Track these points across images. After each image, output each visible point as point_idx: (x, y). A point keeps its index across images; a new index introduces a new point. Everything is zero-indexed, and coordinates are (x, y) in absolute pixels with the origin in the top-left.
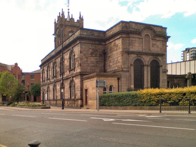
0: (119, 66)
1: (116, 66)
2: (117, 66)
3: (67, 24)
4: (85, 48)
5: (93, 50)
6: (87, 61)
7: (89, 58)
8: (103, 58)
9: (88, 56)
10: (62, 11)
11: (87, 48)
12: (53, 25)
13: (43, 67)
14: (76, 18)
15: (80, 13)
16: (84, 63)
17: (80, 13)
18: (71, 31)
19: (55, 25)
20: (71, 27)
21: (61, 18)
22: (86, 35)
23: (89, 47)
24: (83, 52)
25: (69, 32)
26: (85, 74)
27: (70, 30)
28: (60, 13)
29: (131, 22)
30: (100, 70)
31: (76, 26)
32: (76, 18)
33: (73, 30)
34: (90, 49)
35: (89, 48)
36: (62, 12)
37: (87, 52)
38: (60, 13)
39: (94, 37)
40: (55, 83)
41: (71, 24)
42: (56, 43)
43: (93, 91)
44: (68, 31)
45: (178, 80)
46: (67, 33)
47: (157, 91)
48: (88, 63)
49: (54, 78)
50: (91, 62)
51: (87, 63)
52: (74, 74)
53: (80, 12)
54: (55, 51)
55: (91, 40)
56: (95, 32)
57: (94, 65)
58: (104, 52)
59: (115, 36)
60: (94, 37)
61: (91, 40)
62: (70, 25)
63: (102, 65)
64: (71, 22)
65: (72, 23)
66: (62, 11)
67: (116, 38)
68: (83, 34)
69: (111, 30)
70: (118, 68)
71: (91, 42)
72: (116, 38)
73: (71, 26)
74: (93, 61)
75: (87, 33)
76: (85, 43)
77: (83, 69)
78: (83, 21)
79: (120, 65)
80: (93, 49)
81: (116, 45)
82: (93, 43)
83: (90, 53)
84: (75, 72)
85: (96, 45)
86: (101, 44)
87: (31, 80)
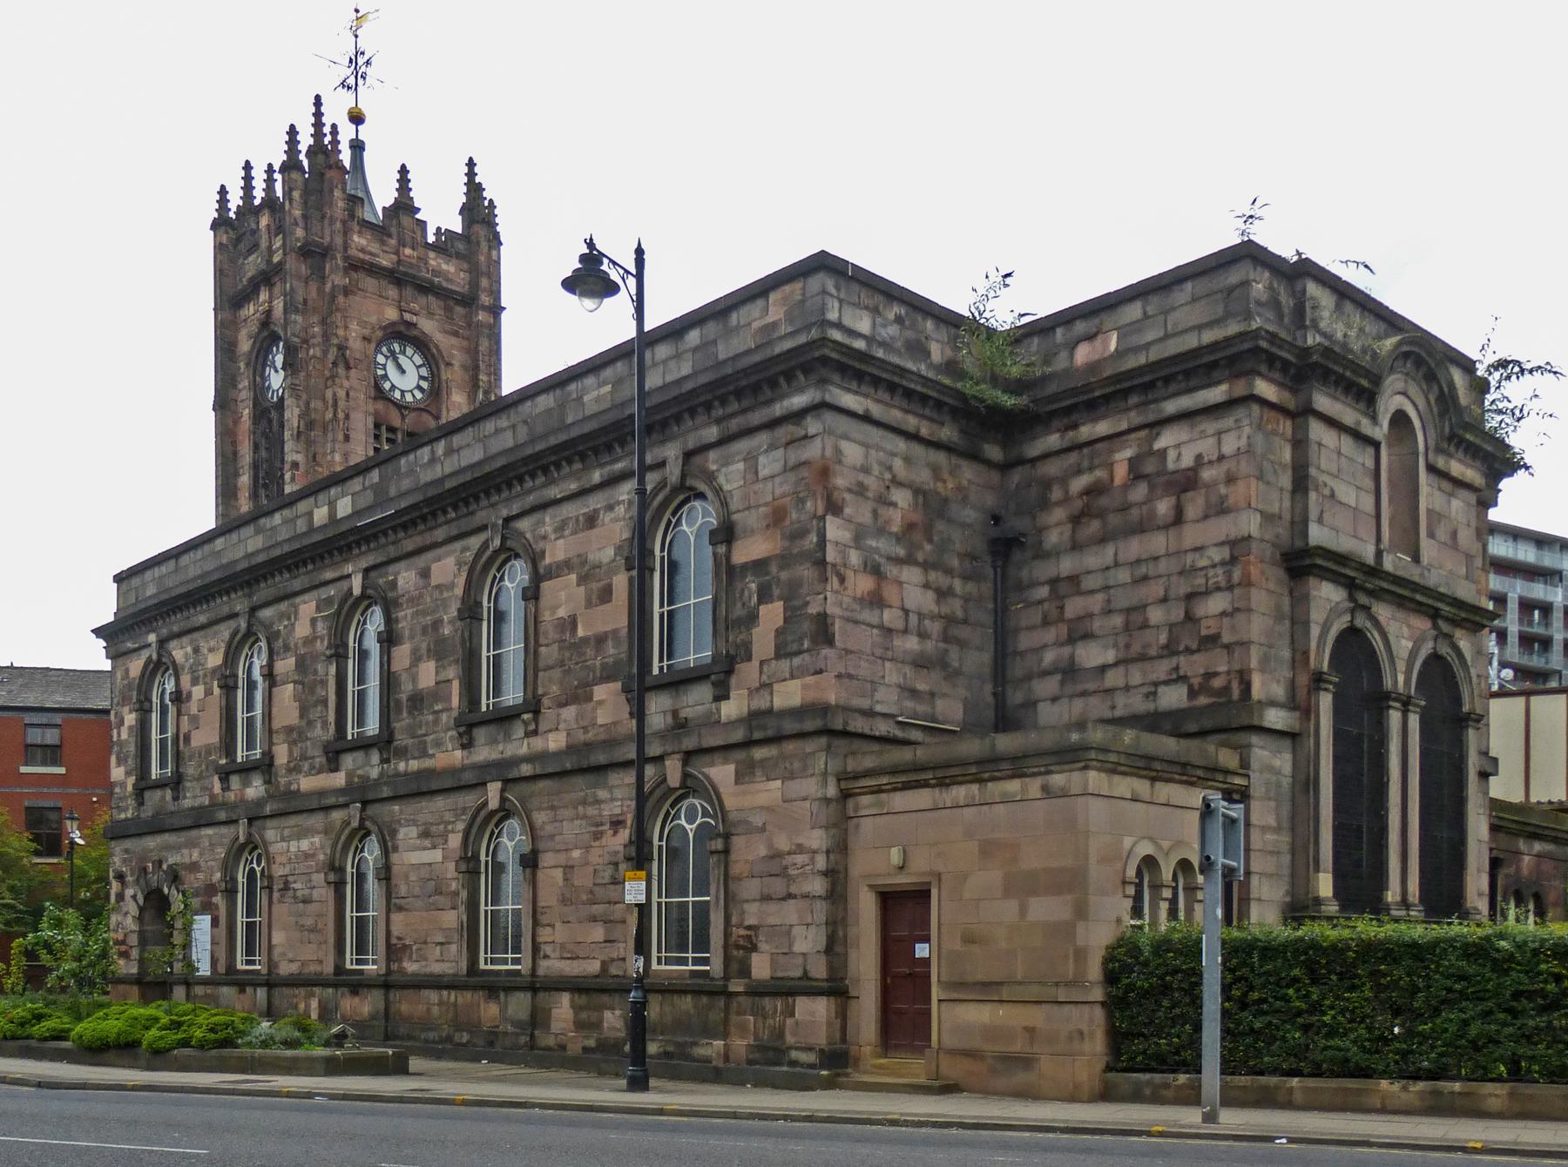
0: (1217, 683)
1: (1167, 683)
2: (1183, 679)
3: (362, 250)
4: (866, 470)
5: (921, 499)
6: (876, 600)
7: (891, 571)
8: (987, 588)
9: (889, 558)
10: (318, 115)
11: (876, 470)
12: (206, 242)
13: (162, 642)
14: (440, 211)
15: (471, 174)
16: (856, 622)
17: (471, 174)
18: (393, 324)
19: (219, 248)
20: (392, 292)
21: (320, 171)
22: (869, 339)
23: (890, 468)
24: (847, 511)
25: (380, 334)
26: (867, 731)
27: (392, 314)
28: (293, 132)
29: (1305, 270)
30: (965, 702)
31: (440, 287)
32: (440, 211)
33: (415, 319)
34: (897, 482)
35: (888, 476)
36: (318, 124)
37: (875, 513)
38: (293, 132)
39: (923, 367)
40: (365, 803)
41: (397, 253)
42: (236, 422)
43: (1023, 911)
44: (373, 319)
45: (1538, 856)
46: (366, 339)
47: (1366, 928)
48: (881, 627)
49: (348, 761)
50: (906, 612)
51: (875, 620)
52: (712, 722)
53: (471, 164)
54: (379, 490)
55: (909, 394)
56: (930, 325)
57: (929, 645)
58: (995, 532)
59: (1167, 380)
60: (924, 373)
61: (909, 394)
62: (385, 261)
63: (978, 659)
64: (393, 242)
65: (408, 251)
66: (318, 115)
67: (1171, 407)
68: (847, 322)
69: (1080, 327)
70: (1203, 700)
71: (911, 422)
72: (1171, 407)
73: (397, 277)
74: (919, 614)
75: (879, 320)
76: (866, 418)
77: (850, 677)
78: (494, 253)
79: (1222, 668)
80: (917, 491)
81: (1162, 471)
82: (924, 432)
83: (896, 520)
84: (731, 709)
85: (940, 457)
86: (974, 456)
87: (23, 769)
